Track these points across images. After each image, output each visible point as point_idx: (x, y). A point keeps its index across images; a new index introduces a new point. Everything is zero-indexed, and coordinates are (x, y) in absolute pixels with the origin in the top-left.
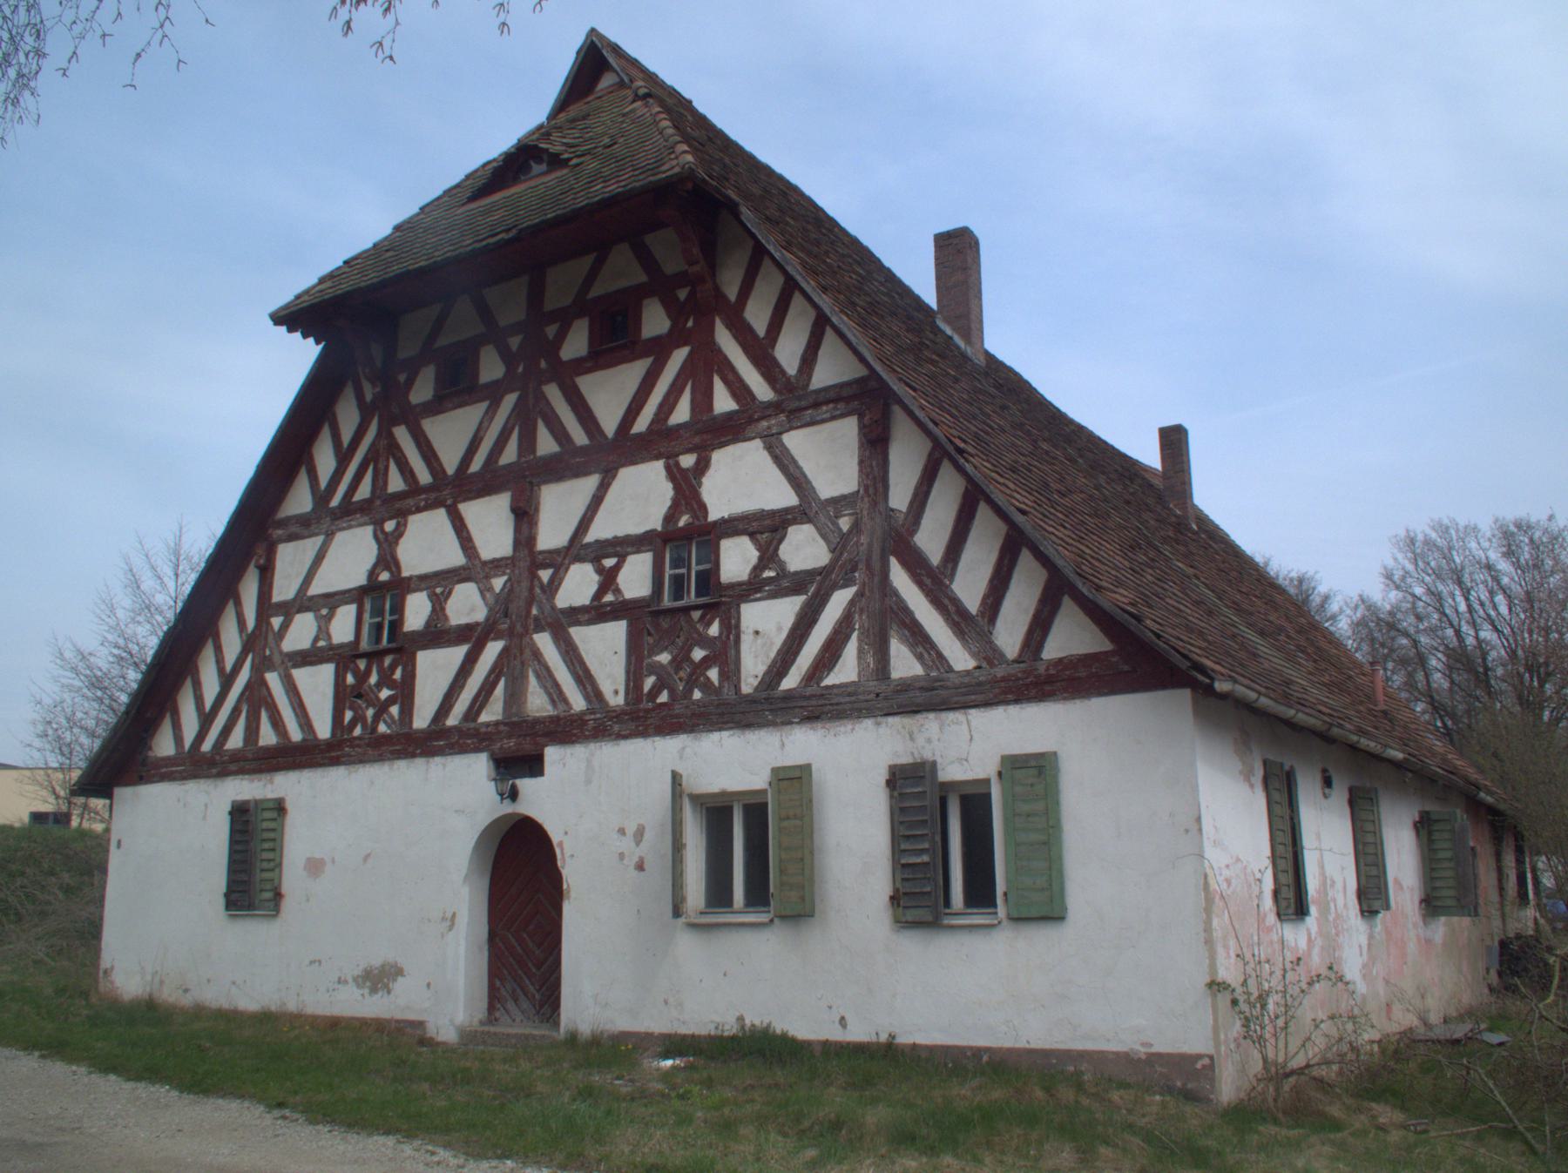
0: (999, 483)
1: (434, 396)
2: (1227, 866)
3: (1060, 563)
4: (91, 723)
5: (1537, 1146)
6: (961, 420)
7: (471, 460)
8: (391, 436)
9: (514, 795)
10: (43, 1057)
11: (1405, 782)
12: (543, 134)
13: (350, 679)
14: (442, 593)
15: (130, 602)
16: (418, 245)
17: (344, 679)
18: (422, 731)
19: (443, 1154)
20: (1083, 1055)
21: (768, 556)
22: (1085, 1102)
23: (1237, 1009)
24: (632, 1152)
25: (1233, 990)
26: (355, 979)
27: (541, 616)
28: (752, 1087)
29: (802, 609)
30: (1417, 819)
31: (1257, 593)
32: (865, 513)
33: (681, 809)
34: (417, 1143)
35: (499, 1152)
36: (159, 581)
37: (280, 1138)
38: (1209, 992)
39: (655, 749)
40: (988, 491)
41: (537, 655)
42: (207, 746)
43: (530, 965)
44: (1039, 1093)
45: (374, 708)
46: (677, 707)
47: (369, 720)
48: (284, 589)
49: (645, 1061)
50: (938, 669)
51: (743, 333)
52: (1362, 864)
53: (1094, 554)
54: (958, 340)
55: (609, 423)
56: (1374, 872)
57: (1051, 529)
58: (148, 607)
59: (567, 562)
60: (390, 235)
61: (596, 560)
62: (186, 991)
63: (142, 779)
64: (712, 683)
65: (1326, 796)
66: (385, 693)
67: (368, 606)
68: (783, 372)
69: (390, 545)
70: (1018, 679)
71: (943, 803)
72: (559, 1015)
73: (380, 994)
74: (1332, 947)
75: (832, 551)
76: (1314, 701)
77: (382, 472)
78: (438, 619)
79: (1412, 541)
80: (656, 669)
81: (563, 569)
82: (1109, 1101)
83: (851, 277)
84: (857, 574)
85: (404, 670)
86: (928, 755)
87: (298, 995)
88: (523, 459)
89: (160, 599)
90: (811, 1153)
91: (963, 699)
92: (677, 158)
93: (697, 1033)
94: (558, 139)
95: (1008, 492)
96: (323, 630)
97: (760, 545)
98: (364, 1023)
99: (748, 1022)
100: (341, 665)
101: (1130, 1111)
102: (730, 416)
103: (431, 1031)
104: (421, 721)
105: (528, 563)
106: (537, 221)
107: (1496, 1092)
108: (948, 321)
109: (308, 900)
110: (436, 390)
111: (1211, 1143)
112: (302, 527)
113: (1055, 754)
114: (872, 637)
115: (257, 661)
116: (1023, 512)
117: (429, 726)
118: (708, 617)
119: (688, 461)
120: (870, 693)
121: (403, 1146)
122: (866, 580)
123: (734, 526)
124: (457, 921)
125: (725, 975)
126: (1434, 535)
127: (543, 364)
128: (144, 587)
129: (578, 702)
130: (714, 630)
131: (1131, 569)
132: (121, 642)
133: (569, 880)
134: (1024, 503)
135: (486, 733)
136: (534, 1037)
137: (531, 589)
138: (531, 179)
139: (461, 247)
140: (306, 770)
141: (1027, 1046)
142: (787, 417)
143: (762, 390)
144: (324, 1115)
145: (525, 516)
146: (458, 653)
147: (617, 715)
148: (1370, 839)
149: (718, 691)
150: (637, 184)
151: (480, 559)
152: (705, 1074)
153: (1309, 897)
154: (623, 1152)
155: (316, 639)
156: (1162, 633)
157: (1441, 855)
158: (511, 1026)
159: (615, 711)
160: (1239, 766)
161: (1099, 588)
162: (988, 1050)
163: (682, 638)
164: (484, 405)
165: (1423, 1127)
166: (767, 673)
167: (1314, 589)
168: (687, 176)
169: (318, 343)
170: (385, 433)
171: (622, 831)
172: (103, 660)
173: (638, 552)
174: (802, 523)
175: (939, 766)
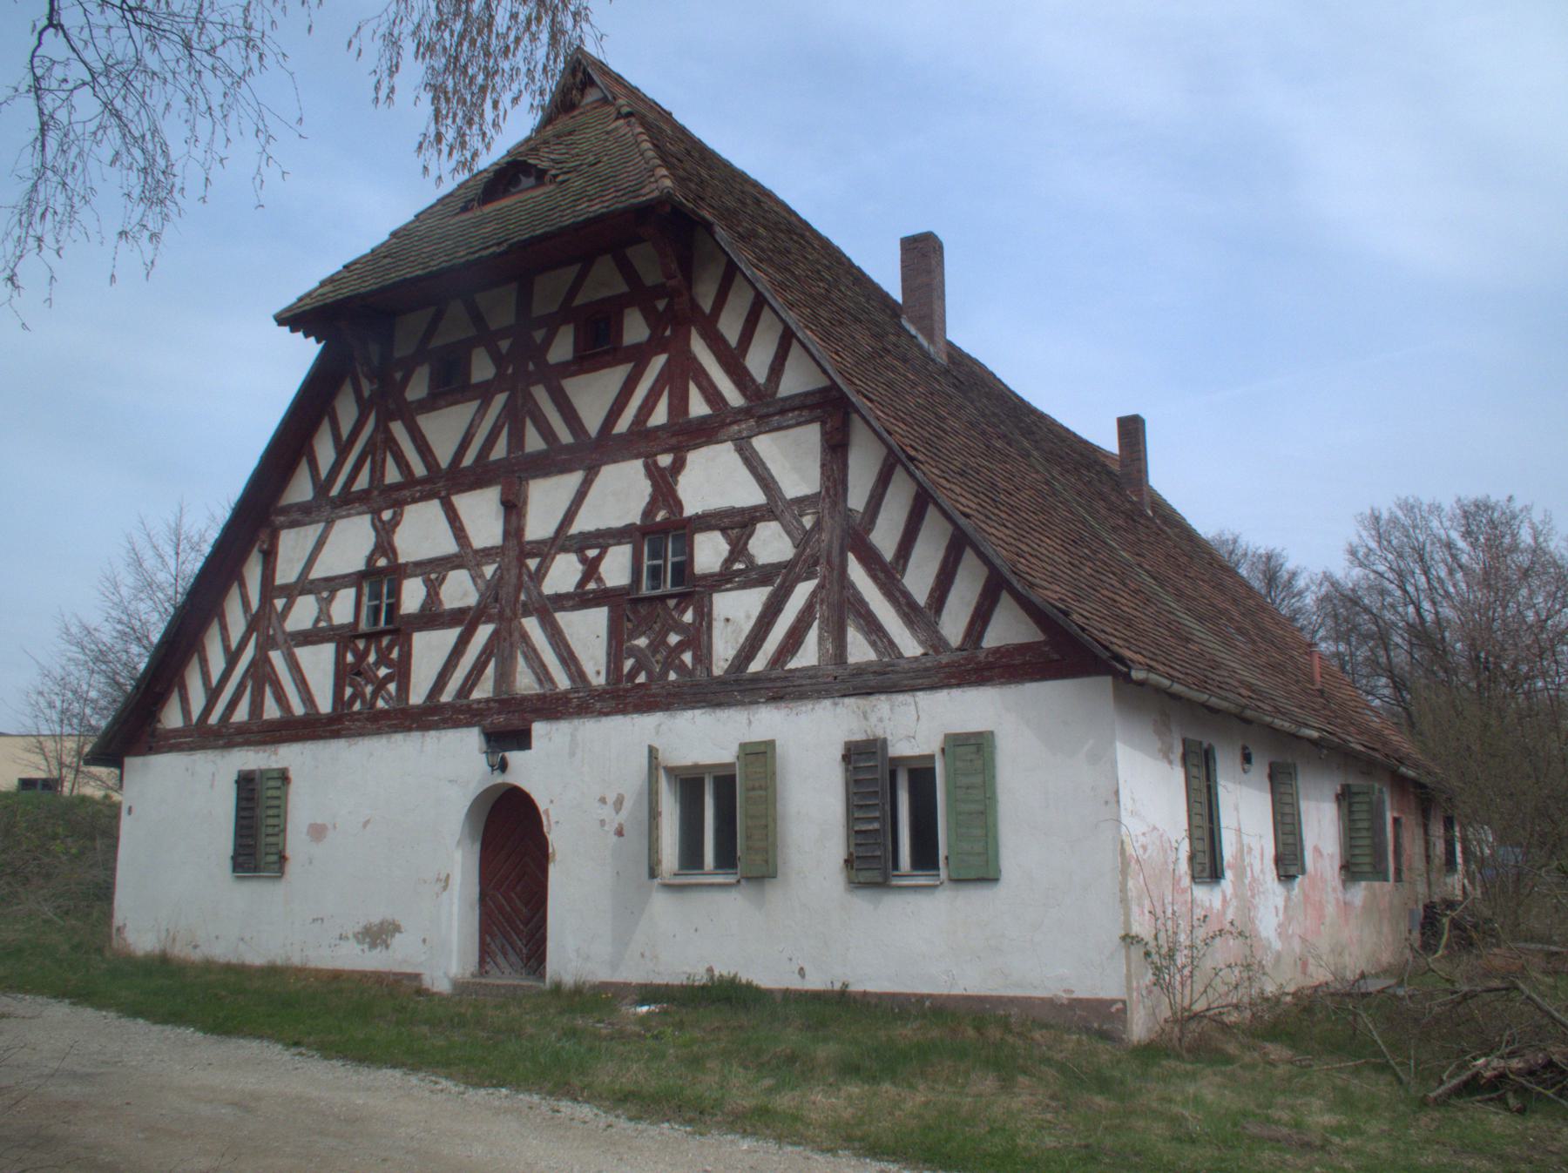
0: (945, 488)
1: (429, 394)
2: (1144, 834)
3: (998, 562)
4: (93, 694)
5: (1403, 1077)
6: (915, 427)
7: (463, 455)
8: (388, 431)
9: (503, 766)
10: (73, 1004)
11: (1320, 758)
12: (532, 150)
13: (350, 658)
14: (437, 578)
15: (132, 580)
16: (413, 254)
17: (344, 657)
18: (418, 707)
19: (444, 1083)
20: (1012, 1001)
21: (738, 550)
22: (1010, 1039)
23: (1150, 960)
24: (612, 1082)
25: (1146, 944)
26: (356, 936)
27: (529, 602)
28: (719, 1028)
29: (769, 599)
30: (1339, 792)
31: (1206, 578)
32: (826, 512)
33: (657, 781)
34: (422, 1075)
35: (495, 1082)
36: (160, 560)
37: (300, 1070)
38: (1123, 944)
39: (633, 725)
40: (935, 496)
41: (525, 637)
42: (213, 719)
43: (518, 922)
44: (971, 1032)
45: (373, 684)
46: (653, 687)
47: (368, 696)
48: (286, 573)
49: (623, 1008)
50: (890, 655)
51: (716, 343)
52: (1280, 832)
53: (1032, 552)
54: (922, 339)
55: (593, 424)
56: (1291, 841)
57: (993, 531)
58: (150, 585)
59: (553, 552)
60: (387, 241)
61: (580, 551)
62: (196, 947)
63: (152, 749)
64: (686, 666)
65: (1245, 771)
66: (383, 672)
67: (366, 590)
68: (753, 380)
69: (387, 533)
70: (960, 665)
71: (893, 775)
72: (545, 967)
73: (379, 949)
74: (1247, 907)
75: (796, 547)
76: (1236, 684)
77: (379, 464)
78: (433, 602)
79: (1377, 519)
80: (633, 652)
81: (548, 560)
82: (1032, 1039)
83: (819, 286)
84: (818, 568)
85: (400, 650)
86: (880, 733)
87: (302, 950)
88: (513, 455)
89: (163, 577)
90: (768, 1082)
91: (911, 682)
92: (656, 181)
93: (670, 983)
94: (546, 155)
95: (954, 496)
96: (324, 613)
97: (731, 540)
98: (363, 976)
99: (717, 973)
100: (342, 644)
101: (1050, 1048)
102: (704, 419)
103: (427, 982)
104: (417, 696)
105: (516, 553)
106: (527, 236)
107: (1374, 1033)
108: (911, 320)
109: (311, 863)
110: (430, 387)
111: (1117, 1074)
112: (303, 515)
113: (992, 733)
114: (831, 625)
115: (261, 639)
116: (967, 516)
117: (425, 702)
118: (683, 605)
119: (665, 460)
120: (828, 676)
121: (408, 1077)
122: (827, 574)
123: (706, 522)
124: (450, 881)
125: (696, 930)
126: (1400, 514)
127: (531, 367)
128: (146, 565)
129: (563, 682)
130: (688, 617)
131: (1070, 563)
132: (125, 618)
133: (555, 846)
134: (968, 507)
135: (477, 710)
136: (521, 987)
137: (520, 576)
138: (520, 192)
139: (455, 258)
140: (309, 742)
141: (964, 993)
142: (756, 422)
143: (733, 396)
144: (337, 1052)
145: (513, 508)
146: (451, 635)
147: (600, 694)
148: (1287, 810)
149: (691, 673)
150: (620, 206)
151: (471, 547)
152: (677, 1018)
153: (1225, 863)
154: (604, 1083)
155: (318, 620)
156: (1086, 627)
157: (1360, 825)
158: (499, 978)
159: (596, 690)
160: (1159, 745)
161: (1032, 585)
162: (930, 996)
163: (659, 624)
164: (474, 405)
165: (1308, 1062)
166: (737, 657)
167: (1282, 565)
168: (665, 200)
169: (318, 341)
170: (382, 428)
171: (603, 800)
172: (107, 634)
173: (619, 543)
174: (769, 521)
175: (889, 743)
